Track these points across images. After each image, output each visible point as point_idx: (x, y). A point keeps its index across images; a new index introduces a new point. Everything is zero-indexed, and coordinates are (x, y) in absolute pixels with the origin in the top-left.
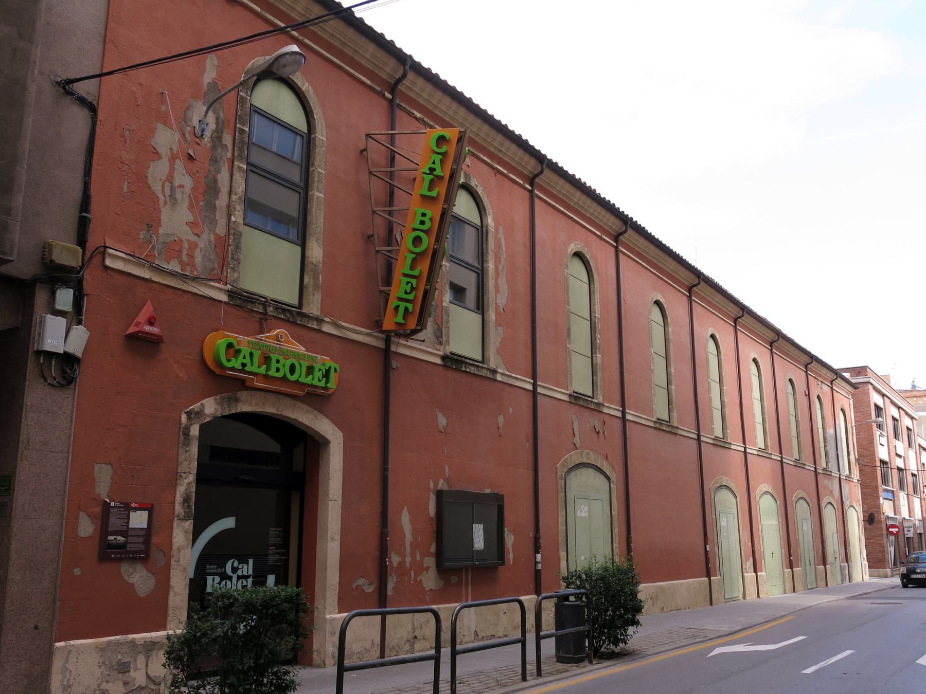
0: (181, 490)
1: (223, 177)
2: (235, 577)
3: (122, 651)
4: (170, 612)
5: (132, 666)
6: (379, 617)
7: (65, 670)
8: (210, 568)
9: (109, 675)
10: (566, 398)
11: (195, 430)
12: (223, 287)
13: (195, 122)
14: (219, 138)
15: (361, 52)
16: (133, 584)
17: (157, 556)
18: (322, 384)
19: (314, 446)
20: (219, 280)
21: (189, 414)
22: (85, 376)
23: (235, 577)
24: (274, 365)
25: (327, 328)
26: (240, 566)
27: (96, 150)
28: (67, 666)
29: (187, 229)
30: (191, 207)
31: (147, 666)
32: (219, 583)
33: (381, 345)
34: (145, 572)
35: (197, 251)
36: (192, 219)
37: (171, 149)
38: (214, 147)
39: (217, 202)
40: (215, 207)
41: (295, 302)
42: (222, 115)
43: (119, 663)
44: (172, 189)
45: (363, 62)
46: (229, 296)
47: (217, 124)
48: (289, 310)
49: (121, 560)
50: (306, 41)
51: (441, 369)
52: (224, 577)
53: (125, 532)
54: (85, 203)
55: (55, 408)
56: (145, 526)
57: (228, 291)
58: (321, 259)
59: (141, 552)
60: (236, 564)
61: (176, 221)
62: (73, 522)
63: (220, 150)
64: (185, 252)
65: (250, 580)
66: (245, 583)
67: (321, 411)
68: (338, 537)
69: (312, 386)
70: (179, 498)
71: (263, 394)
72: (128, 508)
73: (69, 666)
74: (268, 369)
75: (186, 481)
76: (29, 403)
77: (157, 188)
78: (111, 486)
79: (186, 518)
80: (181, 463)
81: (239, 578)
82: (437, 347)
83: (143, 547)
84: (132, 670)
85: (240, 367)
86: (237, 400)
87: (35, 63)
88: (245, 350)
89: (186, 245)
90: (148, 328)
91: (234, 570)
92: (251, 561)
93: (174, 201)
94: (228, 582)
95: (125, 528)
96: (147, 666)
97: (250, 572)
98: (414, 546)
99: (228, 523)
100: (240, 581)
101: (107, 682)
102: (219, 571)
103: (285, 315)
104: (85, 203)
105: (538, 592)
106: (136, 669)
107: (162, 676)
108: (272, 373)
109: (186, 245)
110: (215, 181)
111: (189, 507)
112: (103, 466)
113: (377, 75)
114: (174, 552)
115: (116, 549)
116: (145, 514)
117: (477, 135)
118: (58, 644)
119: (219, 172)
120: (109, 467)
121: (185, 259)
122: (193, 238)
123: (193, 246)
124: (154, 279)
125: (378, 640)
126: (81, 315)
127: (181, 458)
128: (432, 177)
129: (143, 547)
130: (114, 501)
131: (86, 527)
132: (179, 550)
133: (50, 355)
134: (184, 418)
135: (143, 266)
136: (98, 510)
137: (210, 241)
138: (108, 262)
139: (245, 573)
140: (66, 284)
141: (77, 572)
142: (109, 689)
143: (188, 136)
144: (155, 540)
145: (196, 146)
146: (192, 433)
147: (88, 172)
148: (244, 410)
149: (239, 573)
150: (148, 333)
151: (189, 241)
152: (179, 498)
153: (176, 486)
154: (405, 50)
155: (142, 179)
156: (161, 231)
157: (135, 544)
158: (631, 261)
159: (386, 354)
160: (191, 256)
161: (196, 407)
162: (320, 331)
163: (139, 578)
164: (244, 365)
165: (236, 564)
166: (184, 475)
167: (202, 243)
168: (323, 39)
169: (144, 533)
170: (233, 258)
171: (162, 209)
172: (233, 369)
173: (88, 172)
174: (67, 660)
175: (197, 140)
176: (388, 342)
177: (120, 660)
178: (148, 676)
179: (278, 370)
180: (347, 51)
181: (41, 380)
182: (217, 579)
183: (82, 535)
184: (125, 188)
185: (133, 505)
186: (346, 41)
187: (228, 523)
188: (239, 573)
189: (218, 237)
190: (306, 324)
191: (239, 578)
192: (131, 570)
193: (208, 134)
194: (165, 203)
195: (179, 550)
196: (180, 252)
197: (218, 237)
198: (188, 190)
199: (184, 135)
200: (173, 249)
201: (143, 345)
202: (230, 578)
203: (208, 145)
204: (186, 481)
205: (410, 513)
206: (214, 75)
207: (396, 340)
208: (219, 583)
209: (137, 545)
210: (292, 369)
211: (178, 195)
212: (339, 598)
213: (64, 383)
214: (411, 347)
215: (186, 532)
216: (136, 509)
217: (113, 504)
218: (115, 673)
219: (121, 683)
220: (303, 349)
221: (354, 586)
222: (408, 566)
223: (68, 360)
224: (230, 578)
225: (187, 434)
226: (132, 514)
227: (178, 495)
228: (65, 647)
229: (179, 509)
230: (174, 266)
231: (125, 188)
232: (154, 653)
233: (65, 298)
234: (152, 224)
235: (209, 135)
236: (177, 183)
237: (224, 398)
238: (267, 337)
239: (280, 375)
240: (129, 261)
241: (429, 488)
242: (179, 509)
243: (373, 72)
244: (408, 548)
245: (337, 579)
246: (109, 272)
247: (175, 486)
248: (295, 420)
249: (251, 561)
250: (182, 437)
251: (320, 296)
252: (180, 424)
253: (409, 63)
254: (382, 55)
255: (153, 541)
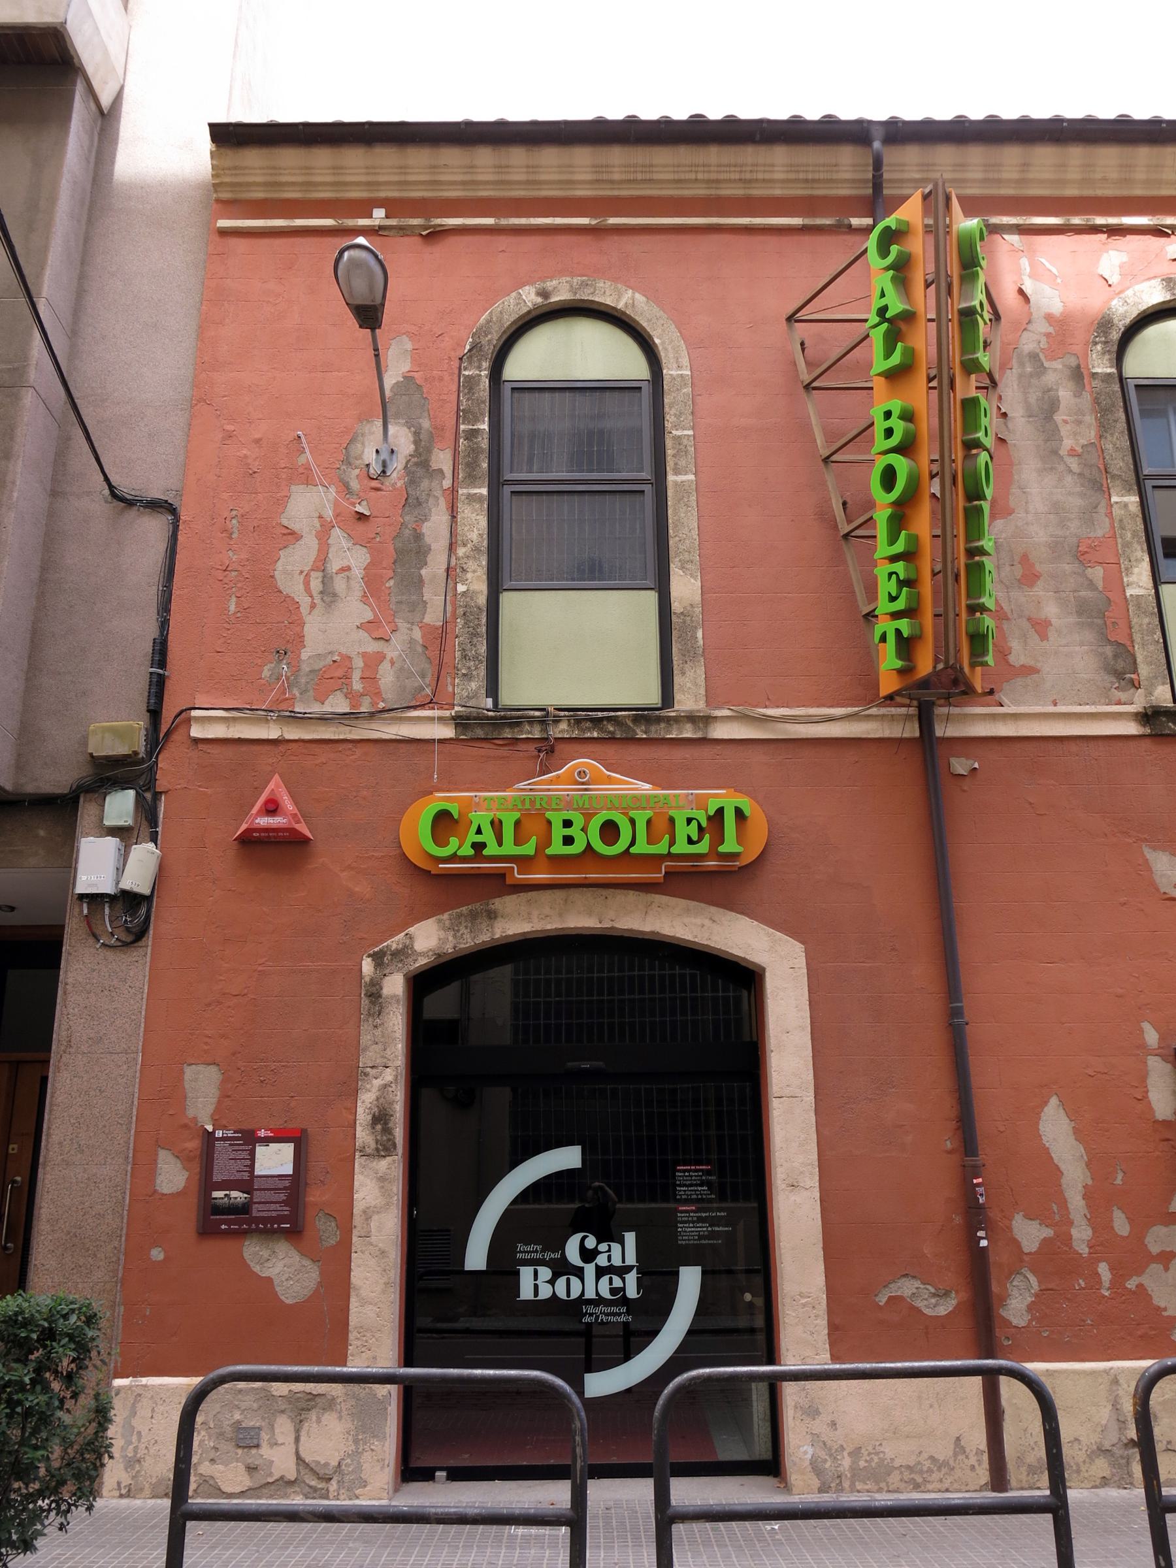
0: (366, 1100)
1: (435, 528)
2: (590, 1270)
3: (243, 1405)
4: (352, 1336)
5: (265, 1436)
6: (975, 1383)
7: (129, 1428)
8: (524, 1250)
9: (216, 1449)
10: (448, 732)
11: (395, 985)
12: (447, 713)
13: (369, 456)
14: (424, 464)
15: (760, 176)
16: (269, 1280)
17: (326, 1231)
18: (703, 847)
19: (745, 979)
20: (430, 703)
21: (378, 958)
22: (164, 924)
23: (590, 1270)
24: (558, 832)
25: (720, 732)
26: (603, 1247)
27: (178, 567)
28: (134, 1422)
29: (363, 634)
30: (364, 599)
31: (297, 1440)
32: (552, 1282)
33: (912, 730)
34: (297, 1258)
35: (385, 667)
36: (369, 616)
37: (320, 517)
38: (413, 482)
39: (423, 572)
40: (421, 581)
41: (653, 697)
42: (426, 424)
43: (237, 1427)
44: (326, 580)
45: (778, 192)
46: (457, 725)
47: (417, 442)
48: (609, 719)
49: (242, 1234)
50: (612, 221)
51: (1146, 744)
52: (562, 1268)
53: (248, 1184)
54: (161, 653)
55: (115, 982)
56: (289, 1170)
57: (453, 718)
58: (698, 598)
59: (280, 1219)
60: (591, 1242)
61: (336, 629)
62: (143, 1167)
63: (425, 484)
64: (356, 676)
65: (632, 1278)
66: (617, 1282)
67: (729, 904)
68: (812, 1181)
69: (670, 856)
70: (363, 1116)
71: (559, 894)
72: (250, 1140)
73: (135, 1422)
74: (672, 842)
75: (377, 1083)
76: (70, 980)
77: (293, 588)
78: (219, 1102)
79: (384, 1149)
80: (366, 1049)
81: (600, 1272)
82: (1123, 696)
83: (286, 1211)
84: (264, 1444)
85: (471, 852)
86: (492, 916)
87: (14, 483)
88: (481, 818)
89: (358, 663)
90: (264, 821)
91: (588, 1255)
92: (630, 1238)
93: (329, 595)
94: (574, 1280)
95: (246, 1176)
96: (297, 1440)
97: (631, 1259)
98: (1099, 1200)
99: (568, 1158)
100: (605, 1280)
101: (212, 1460)
102: (548, 1256)
103: (601, 730)
104: (161, 653)
105: (982, 1338)
106: (274, 1444)
107: (334, 1463)
108: (557, 848)
109: (358, 663)
110: (418, 537)
111: (387, 1130)
112: (201, 1068)
113: (825, 198)
114: (357, 1220)
115: (229, 1215)
116: (288, 1149)
117: (1062, 182)
118: (118, 1382)
119: (425, 518)
120: (213, 1069)
121: (357, 686)
122: (373, 647)
123: (373, 661)
124: (288, 736)
125: (978, 1438)
126: (156, 826)
127: (365, 1039)
128: (885, 325)
129: (286, 1211)
130: (224, 1128)
131: (172, 1176)
132: (367, 1215)
133: (94, 899)
134: (367, 966)
135: (266, 720)
136: (194, 1145)
137: (412, 641)
138: (196, 732)
139: (617, 1261)
140: (122, 784)
141: (157, 1254)
142: (216, 1475)
143: (355, 485)
144: (314, 1196)
145: (373, 494)
146: (386, 991)
147: (165, 607)
148: (510, 933)
149: (602, 1260)
150: (267, 830)
151: (364, 655)
152: (363, 1116)
153: (356, 1092)
154: (611, 116)
155: (262, 583)
156: (305, 655)
157: (267, 1206)
158: (562, 239)
159: (928, 748)
160: (370, 679)
161: (395, 942)
162: (704, 741)
163: (284, 1269)
164: (479, 847)
165: (591, 1242)
166: (372, 1072)
167: (395, 649)
168: (660, 199)
169: (287, 1183)
170: (465, 657)
171: (308, 619)
172: (453, 858)
173: (165, 607)
174: (133, 1413)
175: (374, 484)
176: (925, 718)
177: (239, 1422)
178: (298, 1457)
179: (568, 840)
180: (727, 191)
181: (91, 940)
182: (545, 1273)
183: (165, 1191)
184: (232, 608)
185: (262, 1133)
186: (713, 176)
187: (568, 1158)
188: (602, 1260)
189: (427, 630)
190: (663, 734)
191: (600, 1272)
192: (265, 1253)
193: (397, 466)
194: (313, 606)
195: (367, 1215)
196: (347, 677)
197: (427, 630)
198: (357, 572)
199: (346, 486)
200: (335, 674)
201: (273, 851)
202: (579, 1273)
203: (400, 484)
204: (377, 1083)
205: (1072, 1113)
206: (405, 366)
207: (945, 710)
208: (552, 1282)
209: (273, 1207)
210: (610, 831)
211: (339, 584)
212: (833, 1328)
213: (129, 939)
214: (1016, 717)
215: (382, 1179)
216: (267, 1141)
217: (219, 1134)
218: (226, 1446)
219: (241, 1467)
220: (648, 786)
221: (882, 1299)
222: (1084, 1250)
223: (129, 900)
224: (579, 1273)
225: (375, 994)
226: (260, 1150)
227: (360, 1110)
228: (130, 1387)
229: (364, 1136)
230: (338, 704)
231: (232, 608)
232: (313, 1415)
233: (120, 806)
234: (287, 647)
235: (401, 466)
236: (334, 565)
237: (460, 915)
238: (551, 782)
239: (577, 848)
240: (234, 719)
241: (1143, 1046)
242: (364, 1136)
243: (811, 198)
244: (1076, 1203)
245: (820, 1280)
246: (200, 746)
247: (355, 1093)
248: (653, 933)
249: (630, 1238)
250: (365, 1002)
251: (701, 671)
252: (361, 977)
253: (878, 134)
254: (812, 156)
255: (310, 1199)
